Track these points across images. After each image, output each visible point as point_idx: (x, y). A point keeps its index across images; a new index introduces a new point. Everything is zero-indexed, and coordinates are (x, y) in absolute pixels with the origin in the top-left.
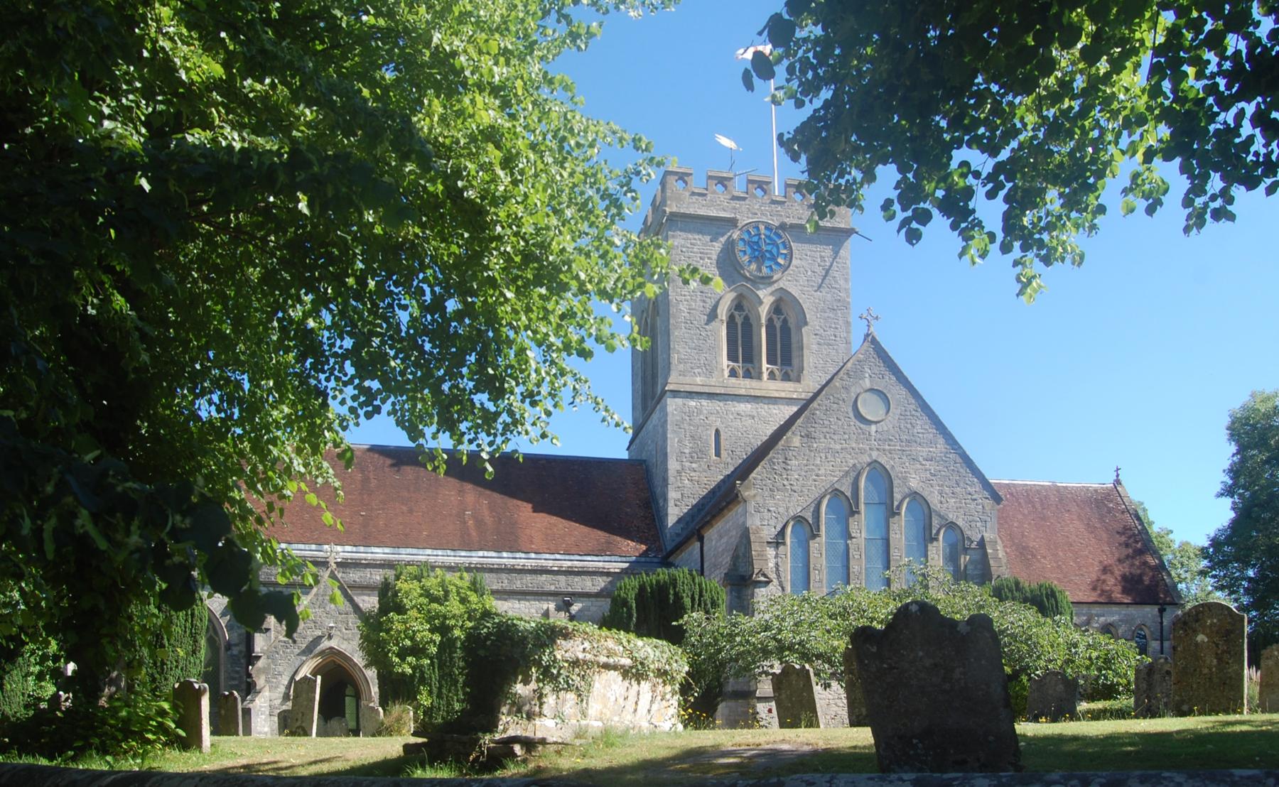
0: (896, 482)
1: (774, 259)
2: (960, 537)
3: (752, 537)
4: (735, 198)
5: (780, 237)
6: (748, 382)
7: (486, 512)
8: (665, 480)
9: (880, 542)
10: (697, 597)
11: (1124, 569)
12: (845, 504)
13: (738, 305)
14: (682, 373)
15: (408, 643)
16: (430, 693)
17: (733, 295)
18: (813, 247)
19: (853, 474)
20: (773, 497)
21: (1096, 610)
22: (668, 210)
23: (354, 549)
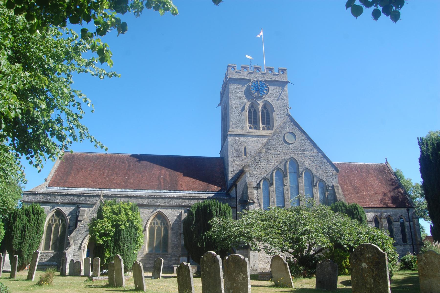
0: (300, 165)
1: (263, 91)
2: (325, 185)
3: (248, 186)
4: (250, 73)
5: (265, 84)
6: (255, 131)
7: (168, 176)
8: (228, 164)
9: (295, 187)
10: (218, 211)
11: (392, 194)
12: (282, 173)
13: (252, 106)
14: (234, 128)
15: (103, 231)
16: (110, 252)
17: (250, 103)
18: (276, 87)
19: (284, 162)
20: (255, 171)
21: (383, 210)
22: (228, 77)
23: (121, 190)
